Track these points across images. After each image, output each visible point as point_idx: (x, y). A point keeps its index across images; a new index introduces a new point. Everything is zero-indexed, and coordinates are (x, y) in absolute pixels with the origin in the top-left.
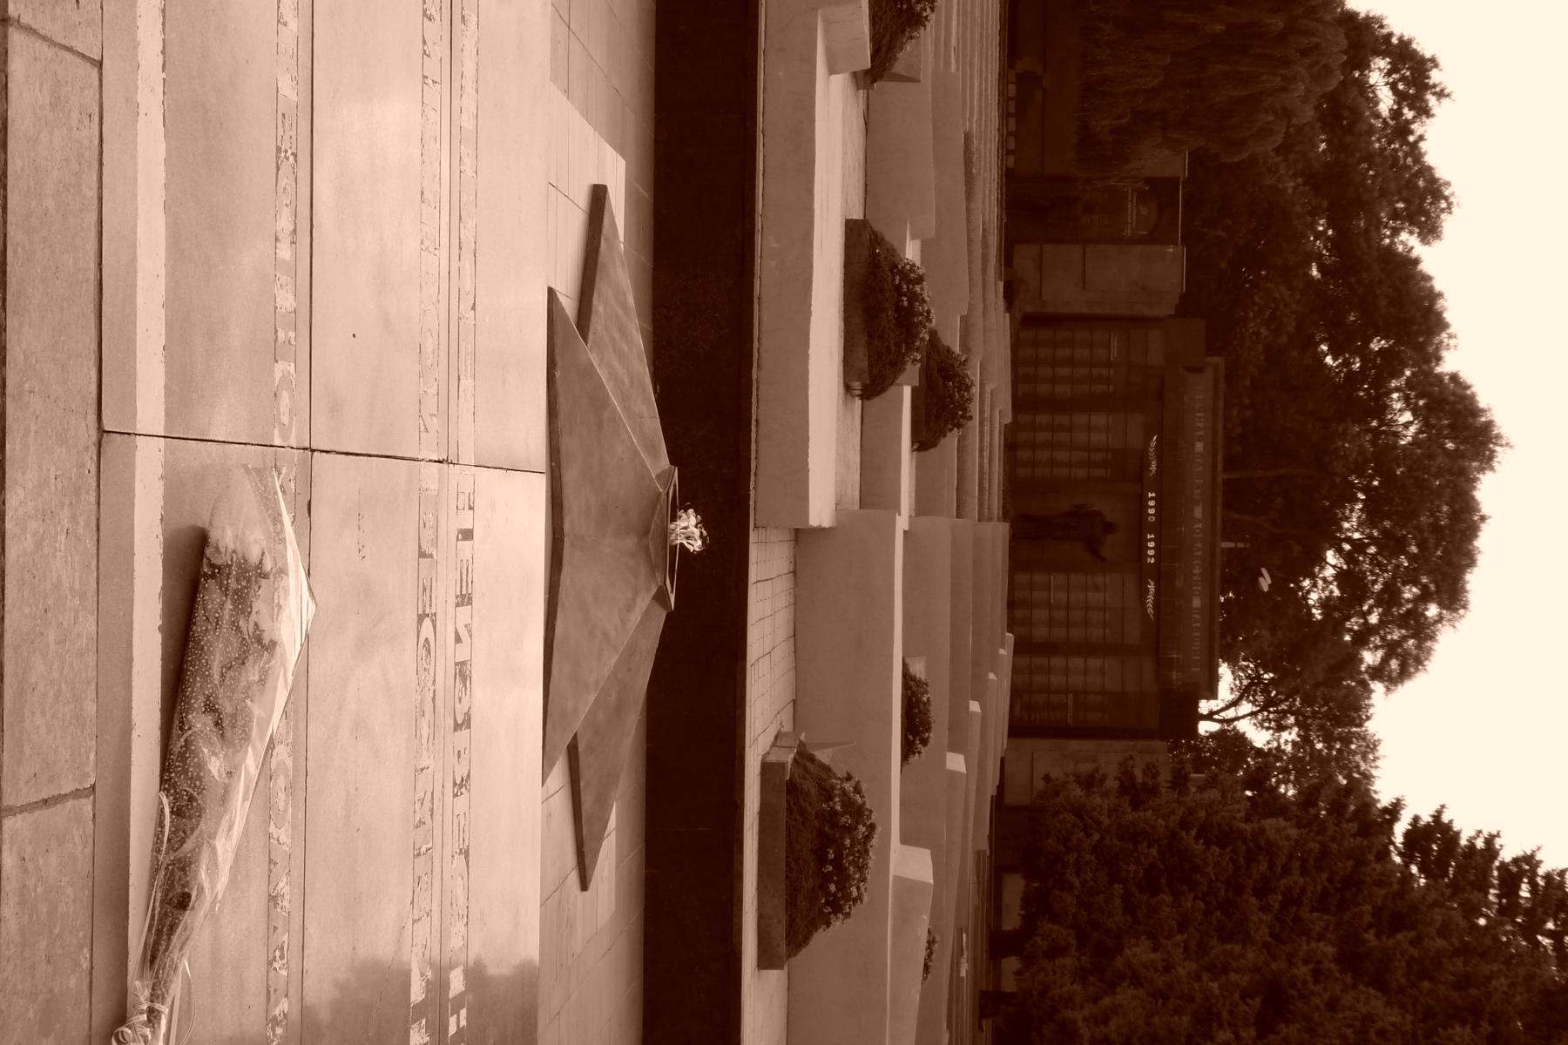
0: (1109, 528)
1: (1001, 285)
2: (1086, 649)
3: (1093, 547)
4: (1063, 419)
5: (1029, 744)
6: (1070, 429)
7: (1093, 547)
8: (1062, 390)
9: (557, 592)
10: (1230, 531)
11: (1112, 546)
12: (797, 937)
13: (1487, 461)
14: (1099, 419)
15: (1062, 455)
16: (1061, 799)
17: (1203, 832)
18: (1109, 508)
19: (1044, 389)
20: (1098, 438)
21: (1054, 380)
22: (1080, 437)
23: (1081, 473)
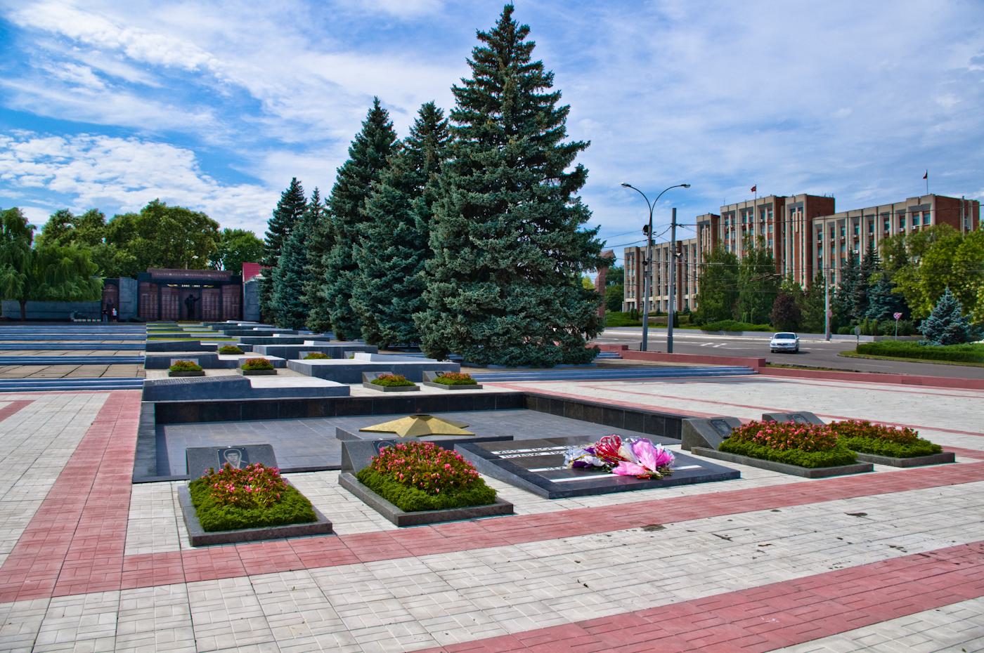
0: (191, 296)
1: (234, 337)
2: (221, 302)
3: (195, 300)
4: (163, 307)
5: (245, 316)
6: (166, 305)
7: (195, 300)
8: (156, 307)
9: (724, 358)
11: (196, 295)
12: (474, 383)
13: (254, 234)
14: (163, 298)
15: (173, 307)
16: (113, 259)
17: (283, 276)
18: (186, 295)
19: (156, 312)
20: (168, 298)
21: (153, 309)
22: (168, 303)
23: (177, 302)
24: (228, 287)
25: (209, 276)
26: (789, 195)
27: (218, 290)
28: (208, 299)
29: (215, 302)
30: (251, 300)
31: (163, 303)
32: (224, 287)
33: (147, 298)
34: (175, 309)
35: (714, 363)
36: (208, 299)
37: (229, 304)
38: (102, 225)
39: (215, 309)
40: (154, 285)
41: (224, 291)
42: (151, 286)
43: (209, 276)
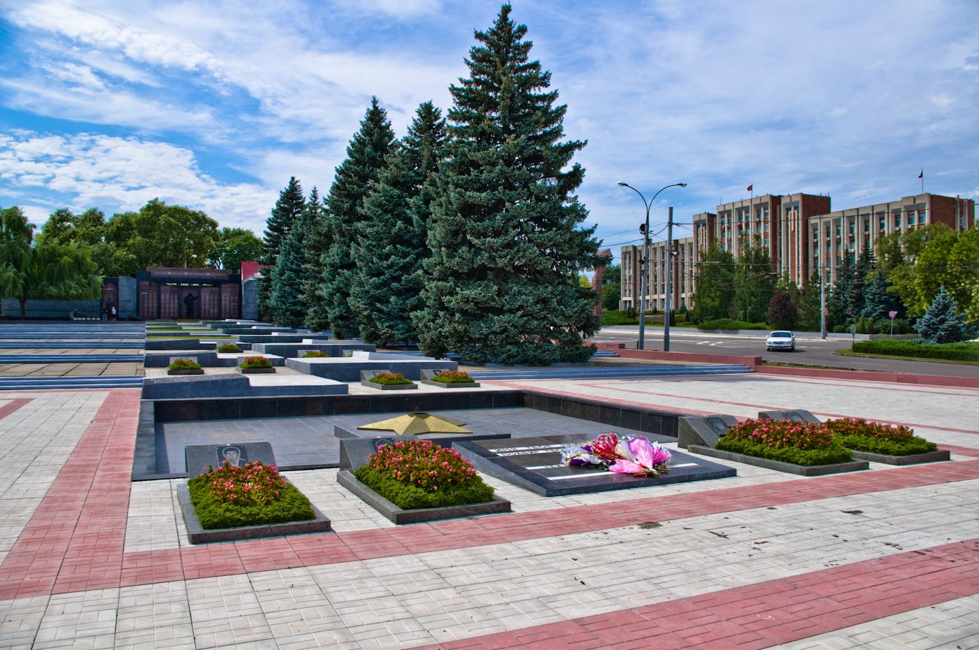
0: (190, 295)
1: (232, 335)
2: (220, 301)
3: (194, 299)
4: (163, 305)
5: (243, 314)
6: (165, 304)
7: (194, 299)
8: (155, 305)
9: (720, 357)
10: (182, 265)
11: (195, 294)
12: (472, 381)
14: (163, 297)
15: (172, 306)
16: (113, 258)
17: (282, 275)
18: (185, 294)
19: (155, 310)
20: (167, 297)
21: (153, 307)
22: (167, 302)
23: (176, 301)
24: (227, 286)
25: (208, 274)
26: (785, 194)
27: (216, 289)
28: (207, 298)
29: (214, 300)
30: (250, 299)
31: (163, 301)
32: (223, 286)
33: (146, 297)
34: (174, 308)
35: (711, 361)
36: (207, 298)
37: (228, 302)
38: (101, 224)
39: (214, 308)
40: (153, 284)
41: (223, 290)
42: (150, 285)
43: (208, 274)
